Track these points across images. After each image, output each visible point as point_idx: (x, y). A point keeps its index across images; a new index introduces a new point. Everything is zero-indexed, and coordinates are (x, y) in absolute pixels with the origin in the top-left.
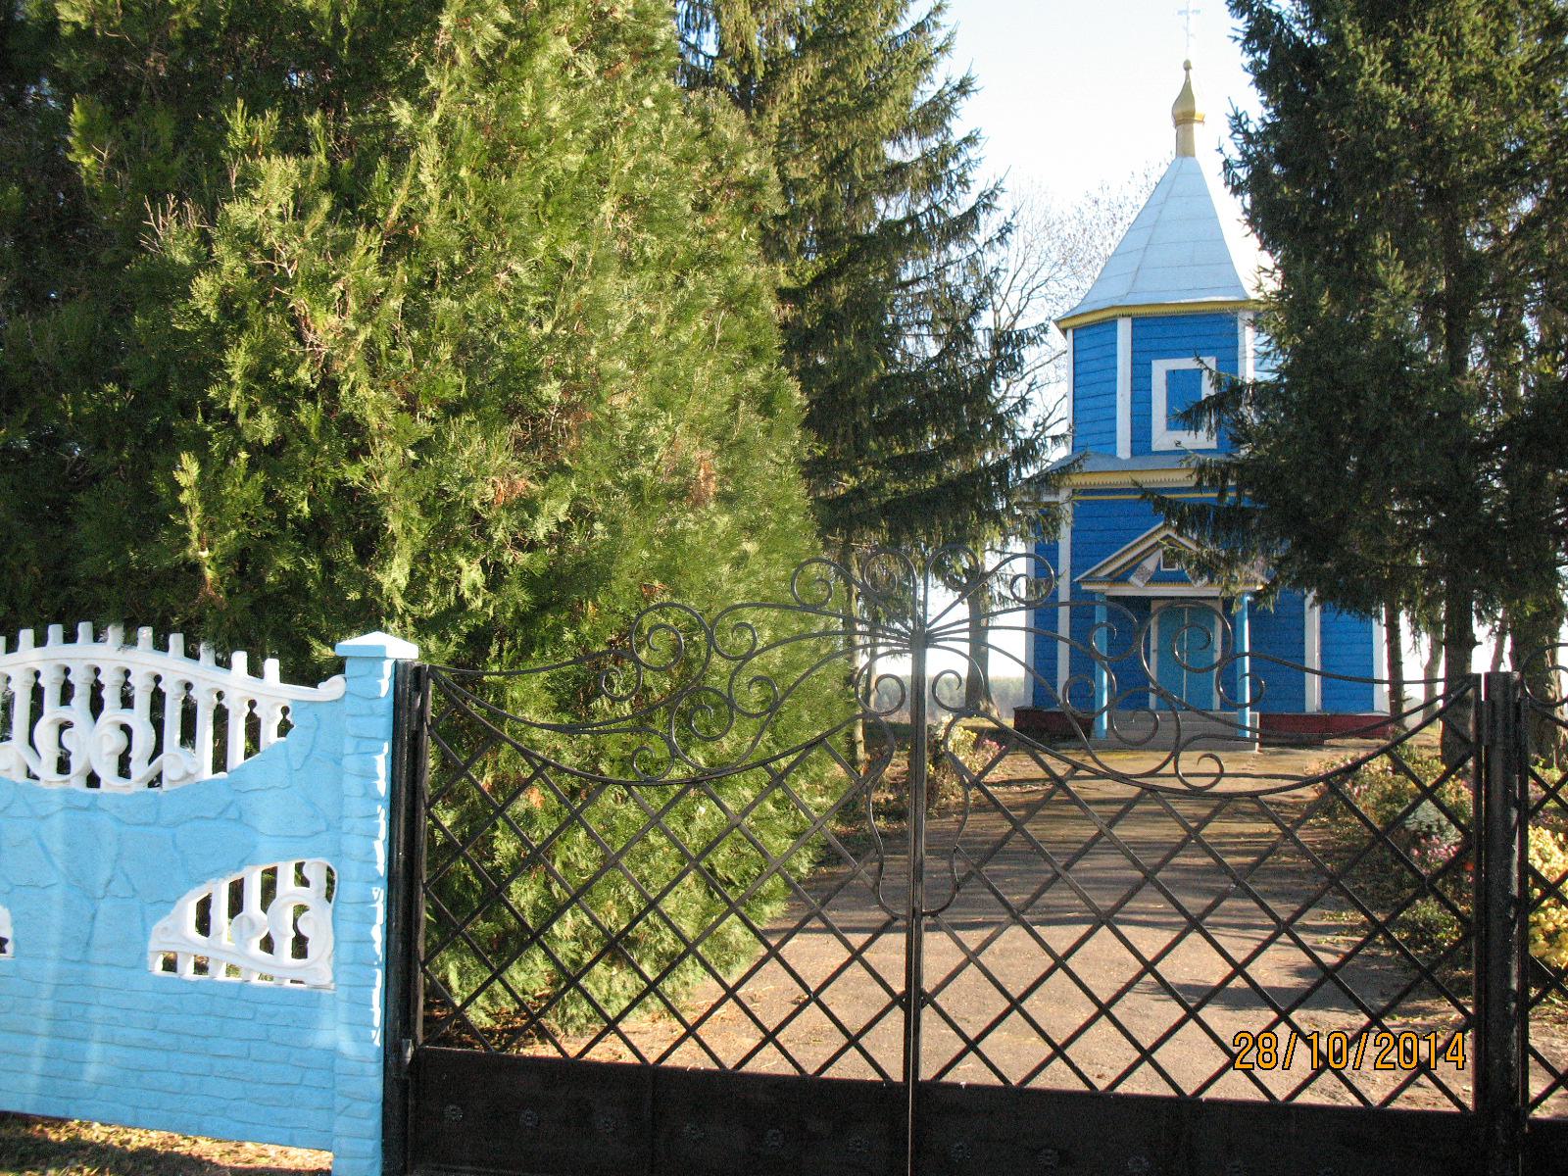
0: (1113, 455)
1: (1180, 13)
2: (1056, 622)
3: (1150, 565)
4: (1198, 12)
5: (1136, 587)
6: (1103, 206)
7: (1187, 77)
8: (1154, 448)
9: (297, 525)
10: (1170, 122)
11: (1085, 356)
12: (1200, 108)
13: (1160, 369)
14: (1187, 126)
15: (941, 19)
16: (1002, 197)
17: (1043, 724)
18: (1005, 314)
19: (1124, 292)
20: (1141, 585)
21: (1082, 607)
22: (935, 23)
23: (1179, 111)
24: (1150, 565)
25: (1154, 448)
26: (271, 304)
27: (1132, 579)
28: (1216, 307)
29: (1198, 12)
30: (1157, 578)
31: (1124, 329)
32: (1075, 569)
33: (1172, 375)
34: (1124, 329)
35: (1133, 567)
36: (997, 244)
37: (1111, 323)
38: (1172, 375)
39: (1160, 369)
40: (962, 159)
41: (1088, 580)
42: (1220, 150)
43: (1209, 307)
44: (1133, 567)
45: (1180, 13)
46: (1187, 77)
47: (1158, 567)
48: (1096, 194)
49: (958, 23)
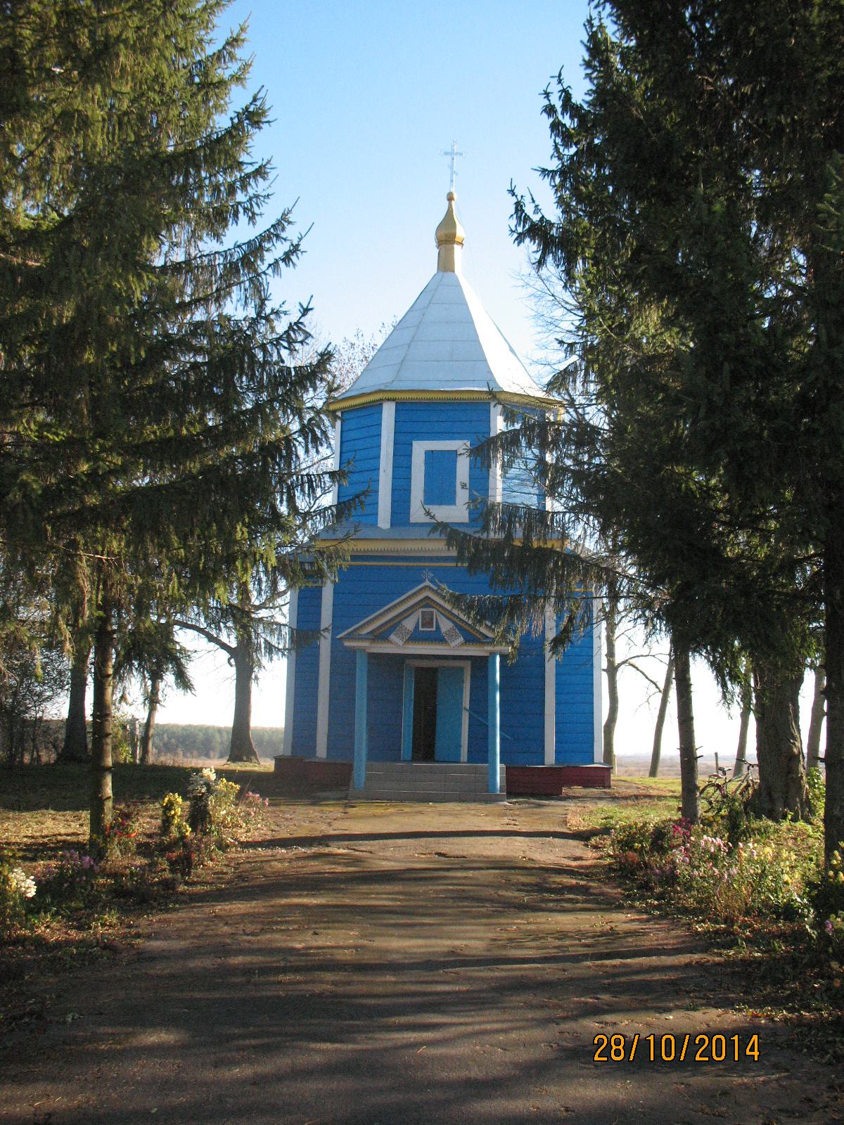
0: (375, 525)
1: (446, 154)
2: (317, 679)
3: (409, 624)
4: (461, 154)
5: (396, 645)
6: (358, 350)
7: (450, 206)
8: (412, 520)
9: (80, 641)
10: (434, 244)
11: (353, 435)
12: (460, 232)
13: (420, 449)
14: (448, 246)
15: (238, 53)
16: (288, 228)
17: (301, 775)
18: (263, 613)
19: (390, 380)
20: (401, 643)
21: (343, 661)
22: (230, 53)
23: (442, 232)
24: (409, 624)
25: (412, 520)
26: (65, 578)
27: (392, 637)
28: (475, 396)
29: (461, 154)
30: (415, 637)
31: (388, 412)
32: (336, 627)
33: (430, 455)
34: (388, 413)
35: (393, 626)
36: (282, 265)
37: (376, 406)
38: (430, 455)
39: (420, 449)
40: (251, 192)
41: (350, 637)
42: (512, 192)
43: (466, 396)
44: (393, 626)
45: (446, 154)
46: (450, 206)
47: (417, 627)
48: (354, 340)
49: (253, 55)
